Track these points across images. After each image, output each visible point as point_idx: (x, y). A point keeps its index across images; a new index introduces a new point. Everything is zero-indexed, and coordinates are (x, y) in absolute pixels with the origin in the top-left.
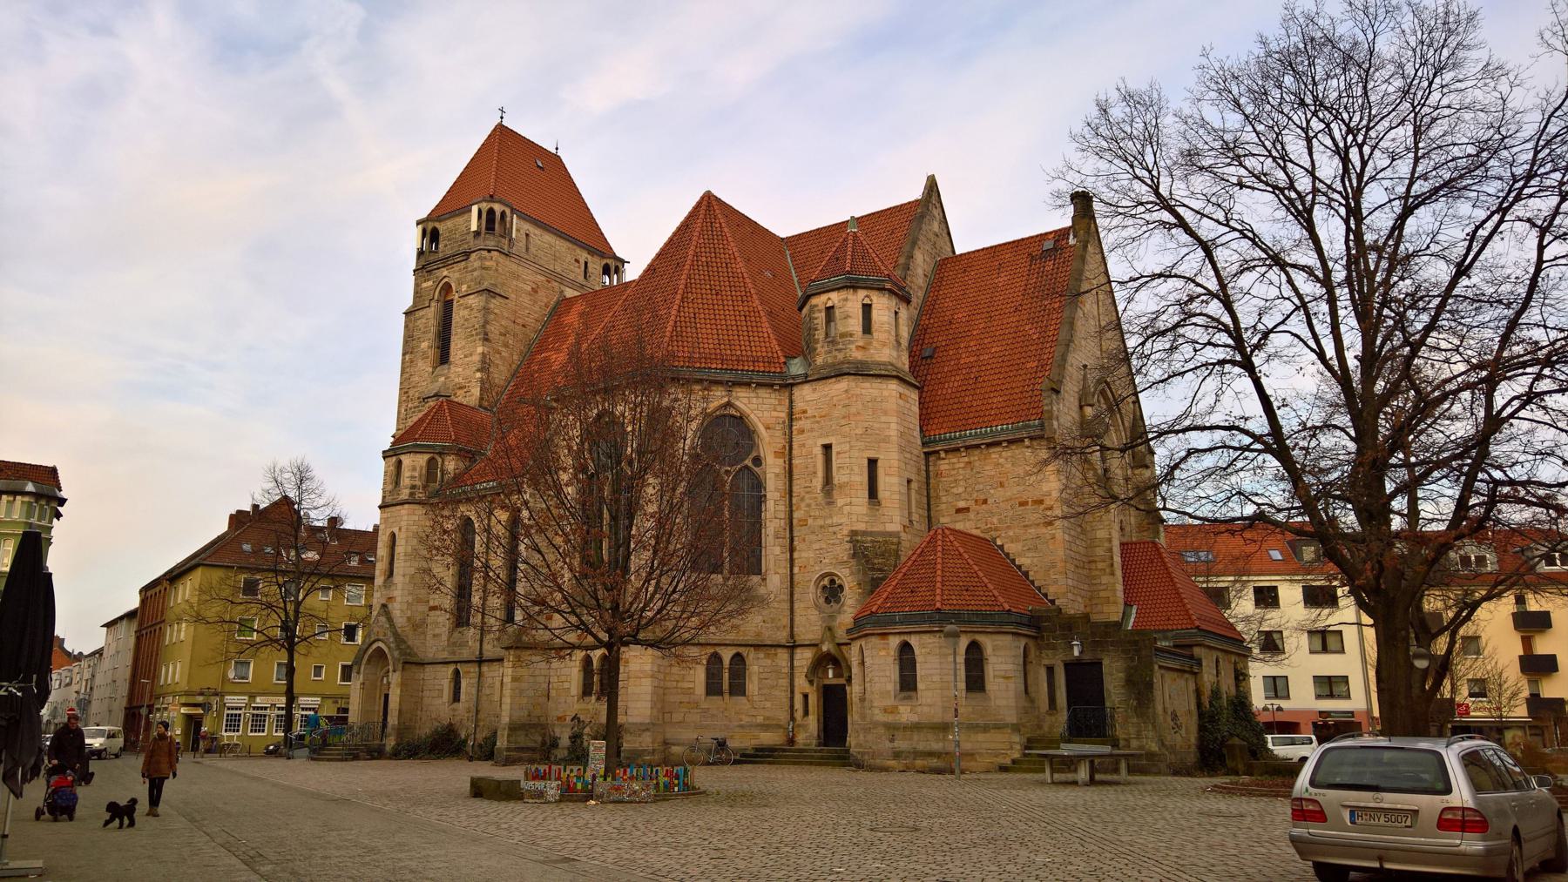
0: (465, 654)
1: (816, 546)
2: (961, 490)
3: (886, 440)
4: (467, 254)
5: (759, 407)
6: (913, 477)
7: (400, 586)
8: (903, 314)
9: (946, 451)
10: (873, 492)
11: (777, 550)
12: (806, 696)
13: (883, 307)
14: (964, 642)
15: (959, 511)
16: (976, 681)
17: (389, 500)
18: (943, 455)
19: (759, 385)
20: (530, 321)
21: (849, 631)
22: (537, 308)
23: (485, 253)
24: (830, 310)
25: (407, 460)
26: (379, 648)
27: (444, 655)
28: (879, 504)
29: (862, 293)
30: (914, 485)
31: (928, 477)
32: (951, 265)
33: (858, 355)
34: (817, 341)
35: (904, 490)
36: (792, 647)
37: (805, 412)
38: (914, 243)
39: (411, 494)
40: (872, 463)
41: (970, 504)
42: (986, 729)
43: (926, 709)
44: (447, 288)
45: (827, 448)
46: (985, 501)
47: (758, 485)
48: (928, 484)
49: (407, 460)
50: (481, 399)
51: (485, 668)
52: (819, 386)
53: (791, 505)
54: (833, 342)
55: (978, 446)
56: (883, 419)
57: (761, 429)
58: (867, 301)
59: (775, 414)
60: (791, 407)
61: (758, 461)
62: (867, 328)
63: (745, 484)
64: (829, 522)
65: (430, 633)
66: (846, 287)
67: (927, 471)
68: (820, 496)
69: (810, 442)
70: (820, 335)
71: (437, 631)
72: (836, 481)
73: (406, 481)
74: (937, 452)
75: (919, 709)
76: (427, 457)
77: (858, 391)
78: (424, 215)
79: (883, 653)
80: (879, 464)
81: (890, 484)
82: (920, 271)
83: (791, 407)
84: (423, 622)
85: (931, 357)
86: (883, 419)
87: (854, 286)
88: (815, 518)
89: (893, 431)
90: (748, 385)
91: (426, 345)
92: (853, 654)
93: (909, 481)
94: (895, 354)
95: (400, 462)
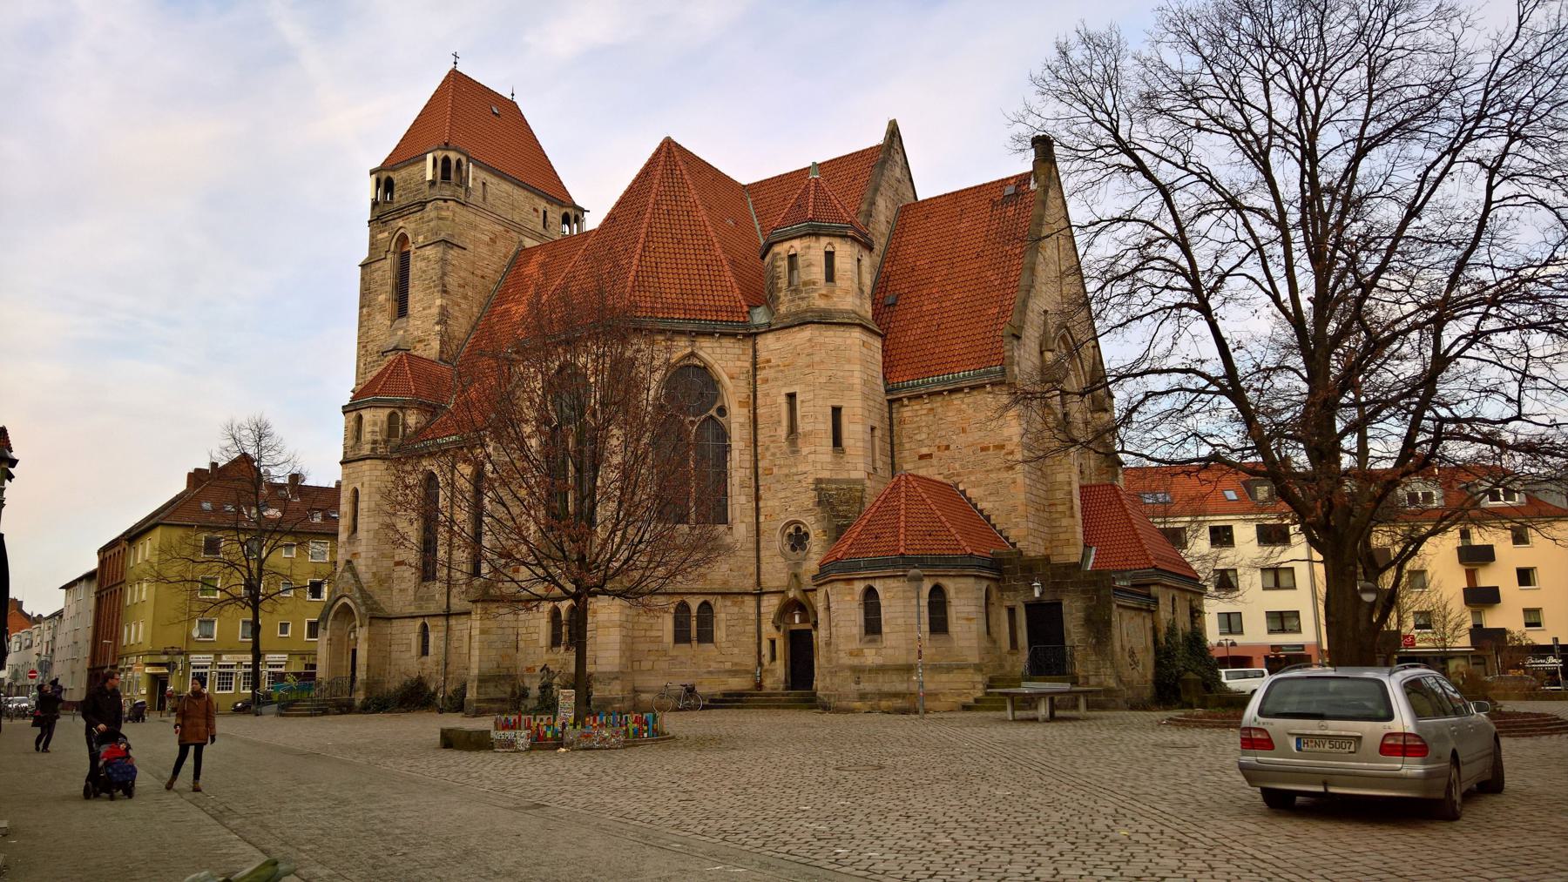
0: (433, 608)
1: (782, 495)
2: (924, 436)
3: (851, 388)
5: (723, 357)
6: (876, 424)
8: (866, 261)
9: (909, 398)
10: (837, 441)
11: (743, 499)
12: (773, 642)
13: (845, 254)
14: (927, 586)
15: (922, 457)
17: (350, 455)
18: (906, 402)
19: (723, 335)
20: (489, 272)
21: (814, 578)
22: (495, 259)
23: (441, 203)
24: (792, 258)
25: (367, 415)
26: (345, 605)
27: (412, 610)
28: (843, 451)
29: (824, 241)
30: (878, 433)
31: (891, 425)
32: (913, 212)
33: (821, 304)
35: (868, 437)
37: (769, 361)
38: (876, 190)
39: (373, 449)
40: (836, 411)
41: (933, 450)
42: (949, 669)
43: (890, 651)
44: (403, 239)
45: (791, 397)
46: (947, 448)
47: (723, 435)
48: (891, 431)
49: (367, 415)
51: (453, 622)
52: (783, 334)
53: (756, 455)
54: (796, 291)
55: (940, 393)
56: (847, 367)
57: (725, 378)
58: (829, 249)
59: (739, 364)
60: (755, 356)
61: (722, 411)
62: (830, 276)
63: (709, 433)
64: (794, 470)
65: (396, 588)
66: (809, 235)
67: (891, 418)
68: (785, 445)
70: (783, 283)
71: (403, 586)
73: (367, 436)
74: (900, 399)
75: (883, 652)
76: (387, 411)
77: (821, 340)
78: (378, 164)
80: (843, 411)
81: (853, 431)
82: (882, 218)
83: (755, 356)
84: (389, 577)
85: (894, 305)
86: (847, 367)
87: (816, 233)
88: (780, 467)
89: (857, 379)
90: (711, 334)
91: (383, 298)
93: (873, 429)
94: (858, 302)
95: (360, 418)
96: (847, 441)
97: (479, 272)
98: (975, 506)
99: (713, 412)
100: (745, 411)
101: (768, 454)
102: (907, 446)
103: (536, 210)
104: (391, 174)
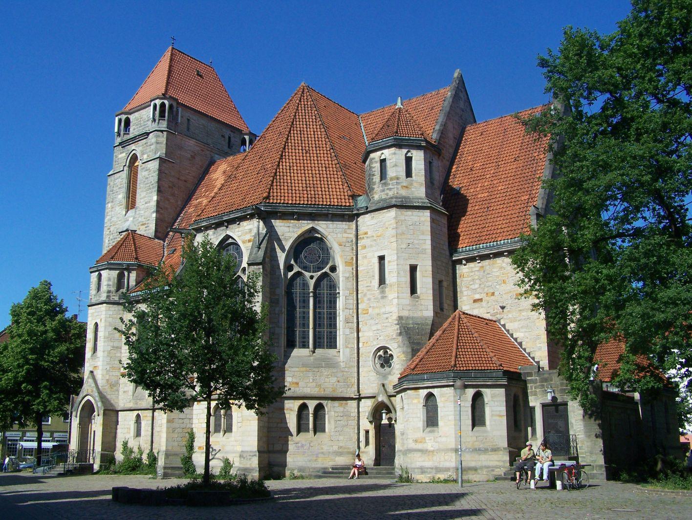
1: (374, 328)
2: (477, 286)
4: (148, 134)
5: (333, 232)
6: (443, 278)
7: (101, 359)
10: (382, 281)
12: (367, 432)
14: (471, 392)
15: (475, 301)
16: (478, 419)
18: (464, 262)
21: (395, 387)
24: (383, 162)
25: (105, 273)
26: (89, 401)
27: (131, 405)
28: (418, 297)
30: (445, 284)
34: (374, 183)
36: (359, 399)
39: (108, 297)
40: (382, 258)
42: (485, 451)
43: (444, 439)
44: (134, 158)
46: (493, 294)
47: (333, 286)
49: (105, 273)
50: (156, 231)
51: (151, 411)
56: (421, 237)
59: (345, 235)
61: (333, 269)
64: (383, 310)
69: (370, 255)
71: (126, 389)
72: (387, 282)
73: (104, 288)
75: (439, 439)
79: (415, 401)
86: (421, 237)
92: (397, 401)
96: (390, 278)
97: (183, 178)
98: (512, 335)
99: (326, 269)
100: (350, 268)
101: (365, 299)
102: (465, 293)
103: (223, 136)
104: (129, 116)
